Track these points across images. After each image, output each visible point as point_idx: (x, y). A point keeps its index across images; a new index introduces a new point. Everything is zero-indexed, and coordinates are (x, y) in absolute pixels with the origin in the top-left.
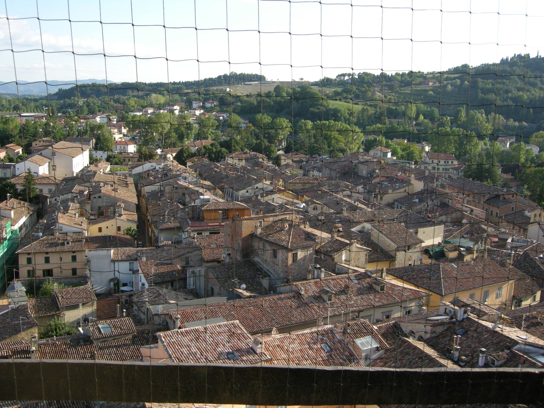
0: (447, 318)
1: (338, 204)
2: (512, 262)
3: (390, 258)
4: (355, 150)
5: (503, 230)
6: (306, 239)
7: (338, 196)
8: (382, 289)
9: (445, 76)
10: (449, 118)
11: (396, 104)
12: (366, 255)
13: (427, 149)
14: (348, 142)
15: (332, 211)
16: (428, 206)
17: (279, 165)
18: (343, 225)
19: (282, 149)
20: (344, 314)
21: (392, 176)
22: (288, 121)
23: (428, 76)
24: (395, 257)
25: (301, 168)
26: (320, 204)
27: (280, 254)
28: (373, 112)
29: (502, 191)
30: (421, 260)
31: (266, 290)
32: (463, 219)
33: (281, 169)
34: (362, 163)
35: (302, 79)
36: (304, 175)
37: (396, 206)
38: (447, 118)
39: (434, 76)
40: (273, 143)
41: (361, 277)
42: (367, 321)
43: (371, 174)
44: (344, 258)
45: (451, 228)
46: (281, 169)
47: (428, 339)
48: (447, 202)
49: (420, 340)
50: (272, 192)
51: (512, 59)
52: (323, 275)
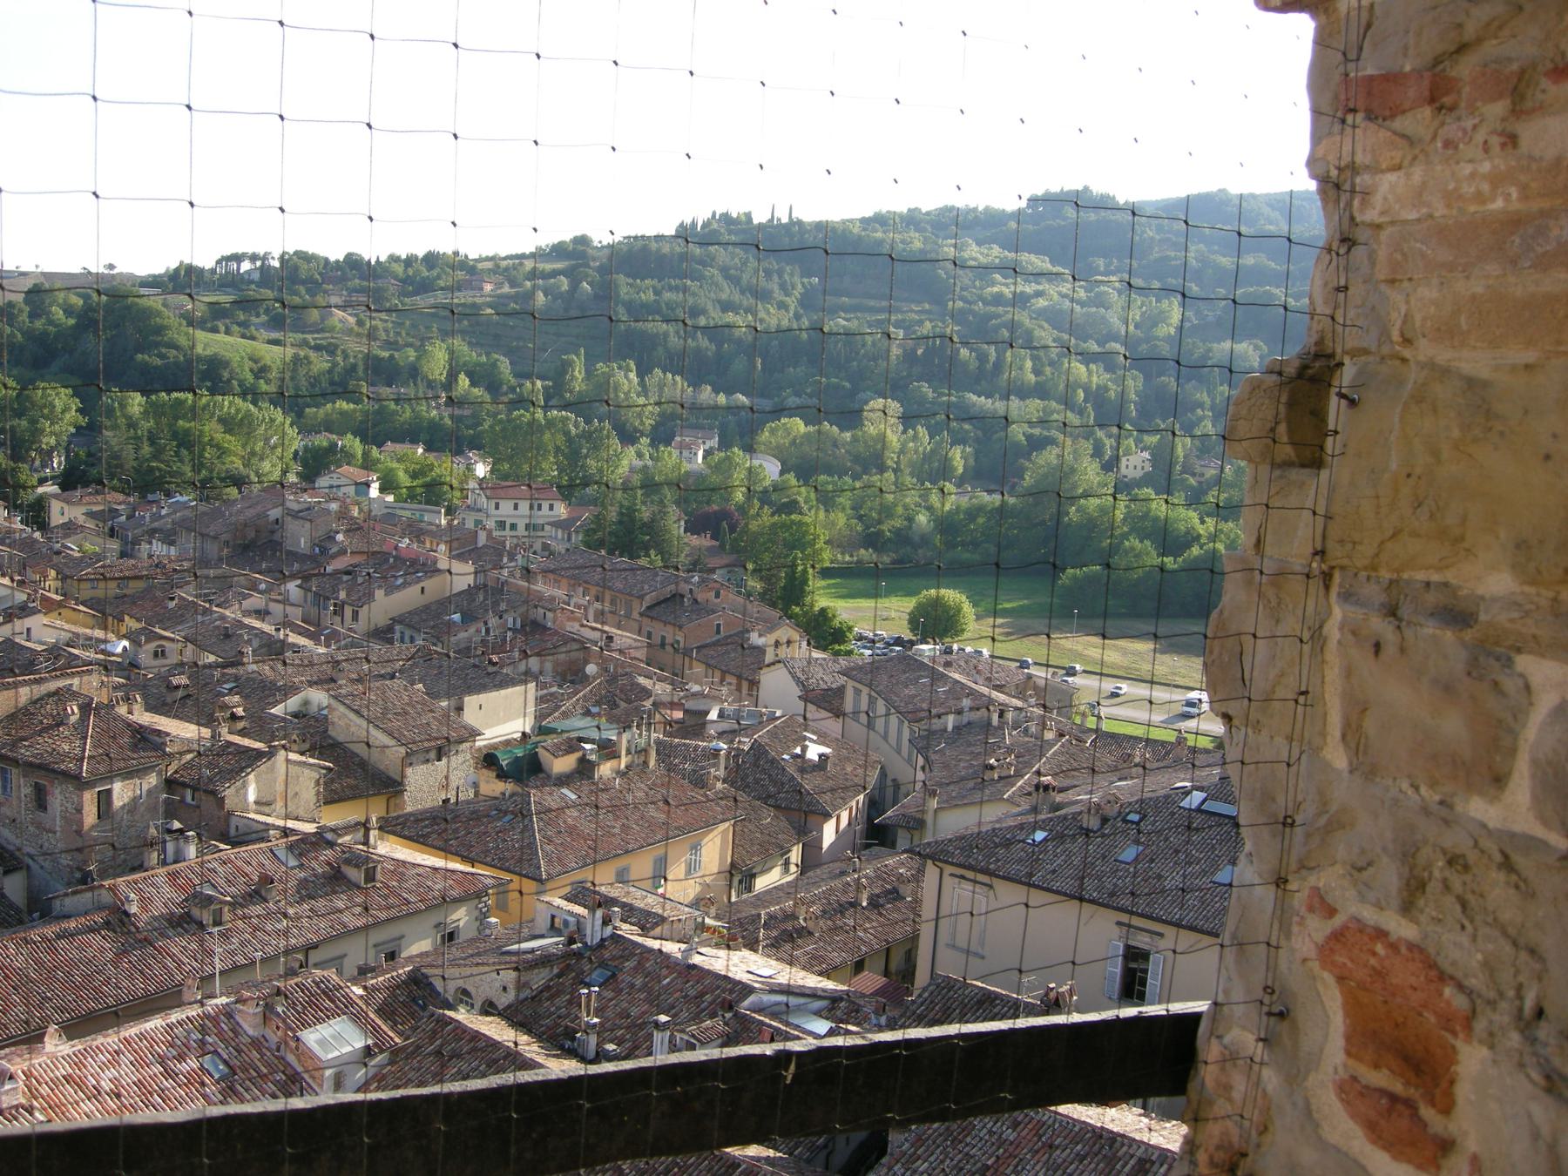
0: (557, 944)
1: (227, 636)
2: (721, 773)
3: (391, 786)
4: (276, 475)
5: (696, 688)
6: (135, 747)
7: (227, 613)
8: (370, 876)
9: (529, 265)
10: (539, 383)
11: (390, 345)
12: (317, 783)
13: (481, 470)
14: (253, 453)
15: (212, 658)
16: (488, 631)
17: (43, 526)
18: (245, 697)
19: (53, 478)
20: (263, 960)
21: (385, 549)
22: (70, 391)
23: (480, 266)
24: (401, 784)
25: (112, 533)
26: (172, 640)
27: (58, 798)
28: (326, 366)
29: (687, 581)
30: (476, 785)
31: (18, 910)
32: (586, 662)
33: (49, 539)
34: (295, 515)
35: (111, 267)
36: (123, 555)
37: (397, 636)
38: (533, 384)
39: (498, 266)
40: (24, 460)
41: (305, 846)
42: (332, 974)
43: (324, 546)
44: (252, 797)
45: (554, 689)
46: (49, 539)
47: (509, 1006)
48: (540, 618)
49: (487, 1014)
50: (24, 611)
51: (706, 225)
52: (192, 851)
